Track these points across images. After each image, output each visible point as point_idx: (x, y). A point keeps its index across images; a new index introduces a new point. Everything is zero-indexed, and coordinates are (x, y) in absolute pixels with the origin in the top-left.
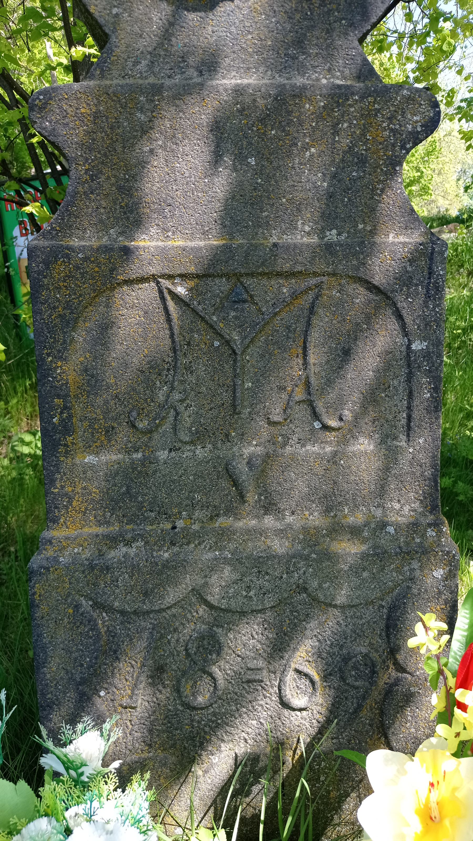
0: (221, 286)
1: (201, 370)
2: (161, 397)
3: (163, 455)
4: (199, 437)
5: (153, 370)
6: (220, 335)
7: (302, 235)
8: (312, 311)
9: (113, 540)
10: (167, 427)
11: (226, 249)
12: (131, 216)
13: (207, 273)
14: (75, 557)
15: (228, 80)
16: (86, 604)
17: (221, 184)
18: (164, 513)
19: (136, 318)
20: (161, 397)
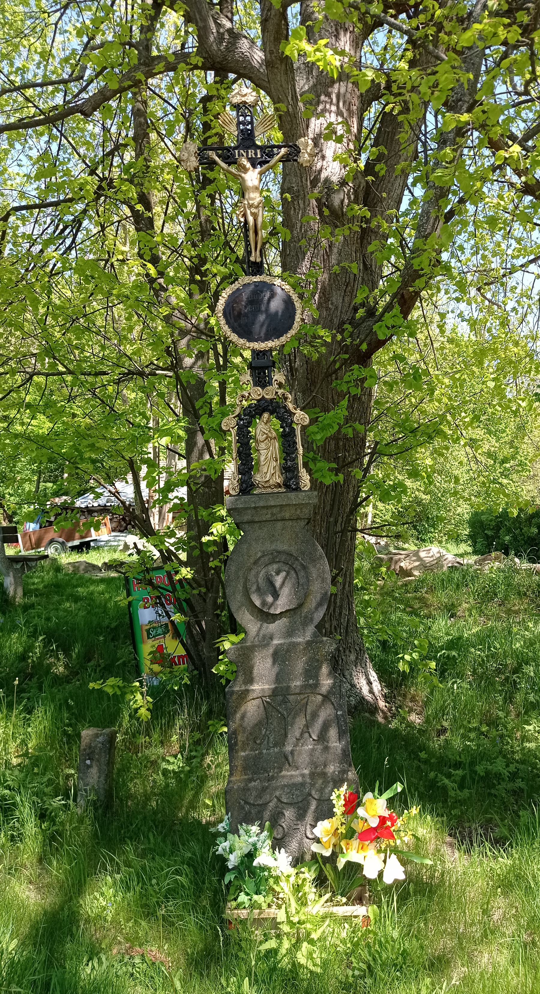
0: (280, 698)
1: (275, 723)
2: (263, 733)
3: (264, 751)
4: (275, 745)
5: (259, 725)
6: (280, 713)
7: (297, 683)
8: (307, 704)
9: (250, 780)
10: (266, 742)
11: (276, 688)
12: (250, 680)
13: (275, 693)
14: (239, 786)
15: (276, 642)
16: (242, 802)
17: (276, 669)
18: (266, 771)
19: (252, 709)
20: (263, 733)
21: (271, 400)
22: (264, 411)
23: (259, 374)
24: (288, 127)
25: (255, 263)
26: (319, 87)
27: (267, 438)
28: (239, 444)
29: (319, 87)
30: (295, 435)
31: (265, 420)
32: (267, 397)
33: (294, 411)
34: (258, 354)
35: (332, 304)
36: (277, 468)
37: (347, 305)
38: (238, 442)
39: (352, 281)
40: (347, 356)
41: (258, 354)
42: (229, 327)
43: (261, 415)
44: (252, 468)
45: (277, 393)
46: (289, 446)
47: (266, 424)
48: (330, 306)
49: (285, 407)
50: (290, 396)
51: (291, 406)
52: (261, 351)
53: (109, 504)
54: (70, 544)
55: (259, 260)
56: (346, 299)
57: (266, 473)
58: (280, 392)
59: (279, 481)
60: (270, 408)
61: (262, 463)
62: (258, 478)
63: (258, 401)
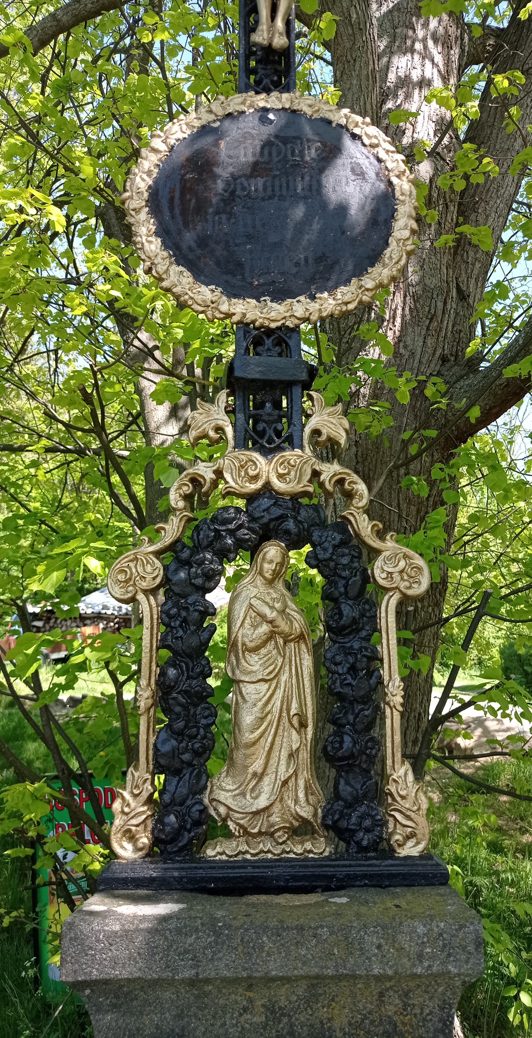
21: (295, 497)
22: (266, 536)
23: (259, 406)
24: (348, 45)
25: (269, 49)
26: (396, 13)
27: (271, 636)
28: (166, 653)
29: (396, 13)
30: (376, 629)
31: (268, 568)
32: (278, 484)
33: (375, 543)
34: (258, 342)
35: (405, 347)
36: (305, 756)
37: (430, 351)
38: (163, 645)
39: (440, 312)
40: (433, 433)
41: (258, 342)
42: (165, 245)
43: (254, 550)
44: (205, 752)
45: (316, 474)
46: (353, 669)
47: (270, 583)
48: (402, 351)
49: (343, 525)
50: (361, 487)
51: (364, 526)
52: (269, 332)
53: (103, 612)
54: (55, 656)
55: (280, 41)
56: (429, 341)
57: (259, 777)
58: (330, 470)
59: (306, 812)
60: (291, 525)
61: (249, 737)
62: (225, 794)
63: (251, 498)
